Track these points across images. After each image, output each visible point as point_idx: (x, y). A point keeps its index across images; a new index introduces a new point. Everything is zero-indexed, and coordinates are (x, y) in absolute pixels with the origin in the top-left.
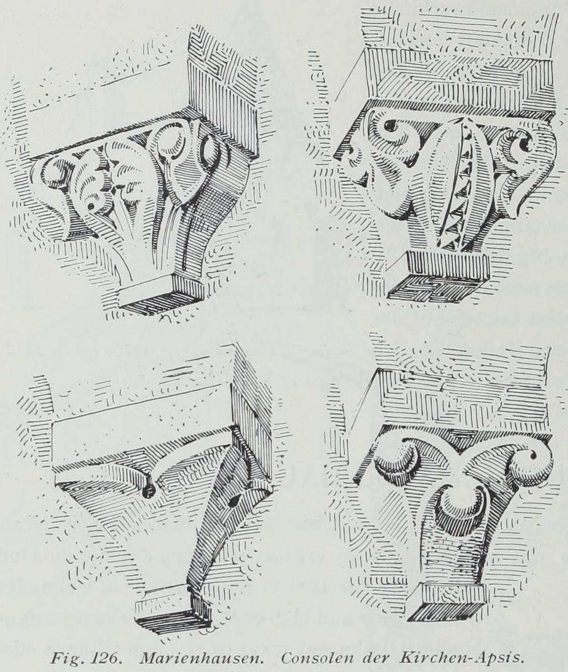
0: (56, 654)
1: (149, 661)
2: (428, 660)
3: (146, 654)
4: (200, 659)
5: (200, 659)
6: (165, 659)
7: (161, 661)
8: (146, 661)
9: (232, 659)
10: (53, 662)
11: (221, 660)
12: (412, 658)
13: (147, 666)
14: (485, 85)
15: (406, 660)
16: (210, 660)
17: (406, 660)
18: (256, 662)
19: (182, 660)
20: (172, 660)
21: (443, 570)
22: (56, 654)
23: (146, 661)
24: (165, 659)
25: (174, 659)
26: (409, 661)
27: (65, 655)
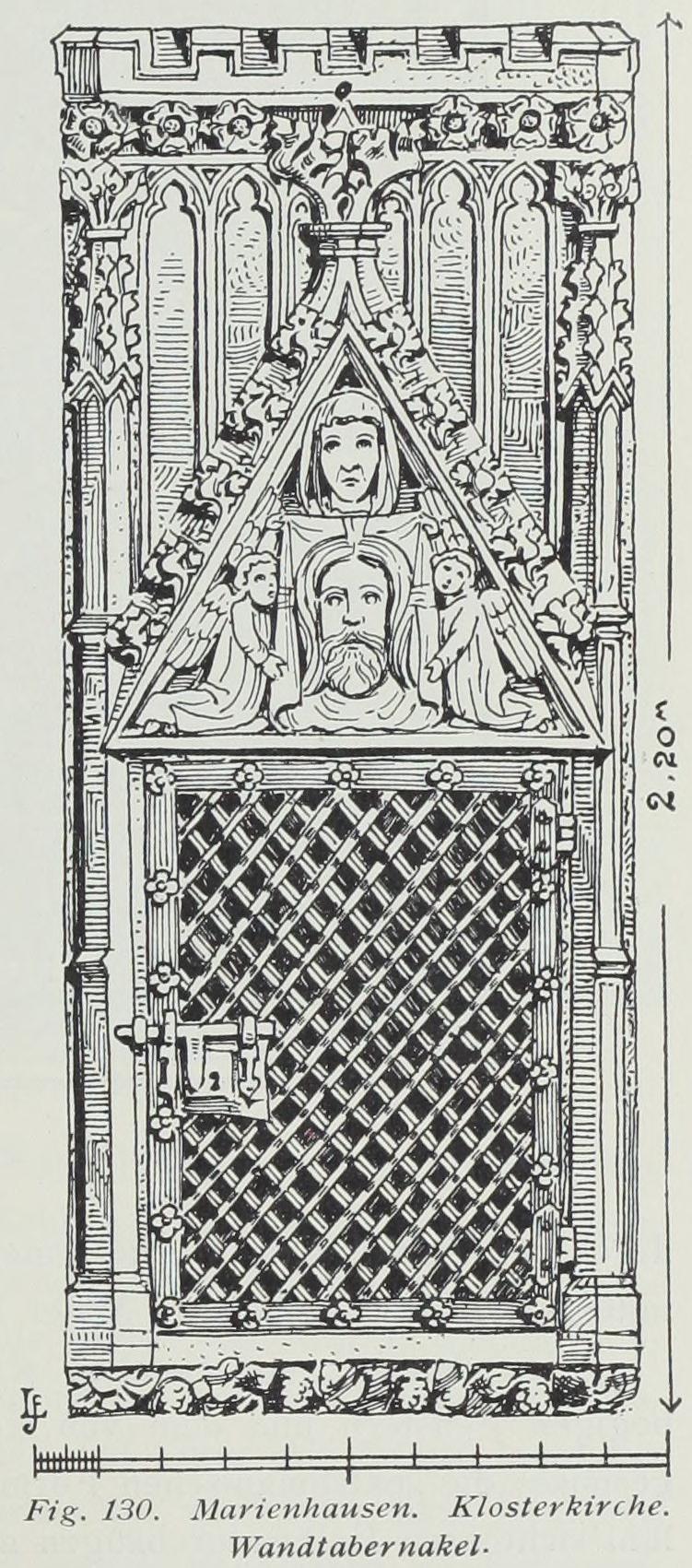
0: (35, 1502)
1: (209, 1515)
2: (609, 1510)
3: (203, 1502)
4: (301, 1511)
5: (301, 1511)
6: (238, 1511)
7: (333, 1515)
8: (204, 1513)
9: (360, 1510)
10: (30, 1518)
11: (339, 1512)
12: (473, 1508)
13: (204, 1523)
14: (240, 342)
15: (461, 1511)
16: (320, 1511)
17: (461, 1511)
18: (405, 1515)
19: (651, 1508)
20: (252, 1513)
21: (138, 435)
22: (35, 1502)
23: (204, 1513)
24: (238, 1511)
25: (254, 1511)
26: (467, 1514)
27: (52, 1504)
